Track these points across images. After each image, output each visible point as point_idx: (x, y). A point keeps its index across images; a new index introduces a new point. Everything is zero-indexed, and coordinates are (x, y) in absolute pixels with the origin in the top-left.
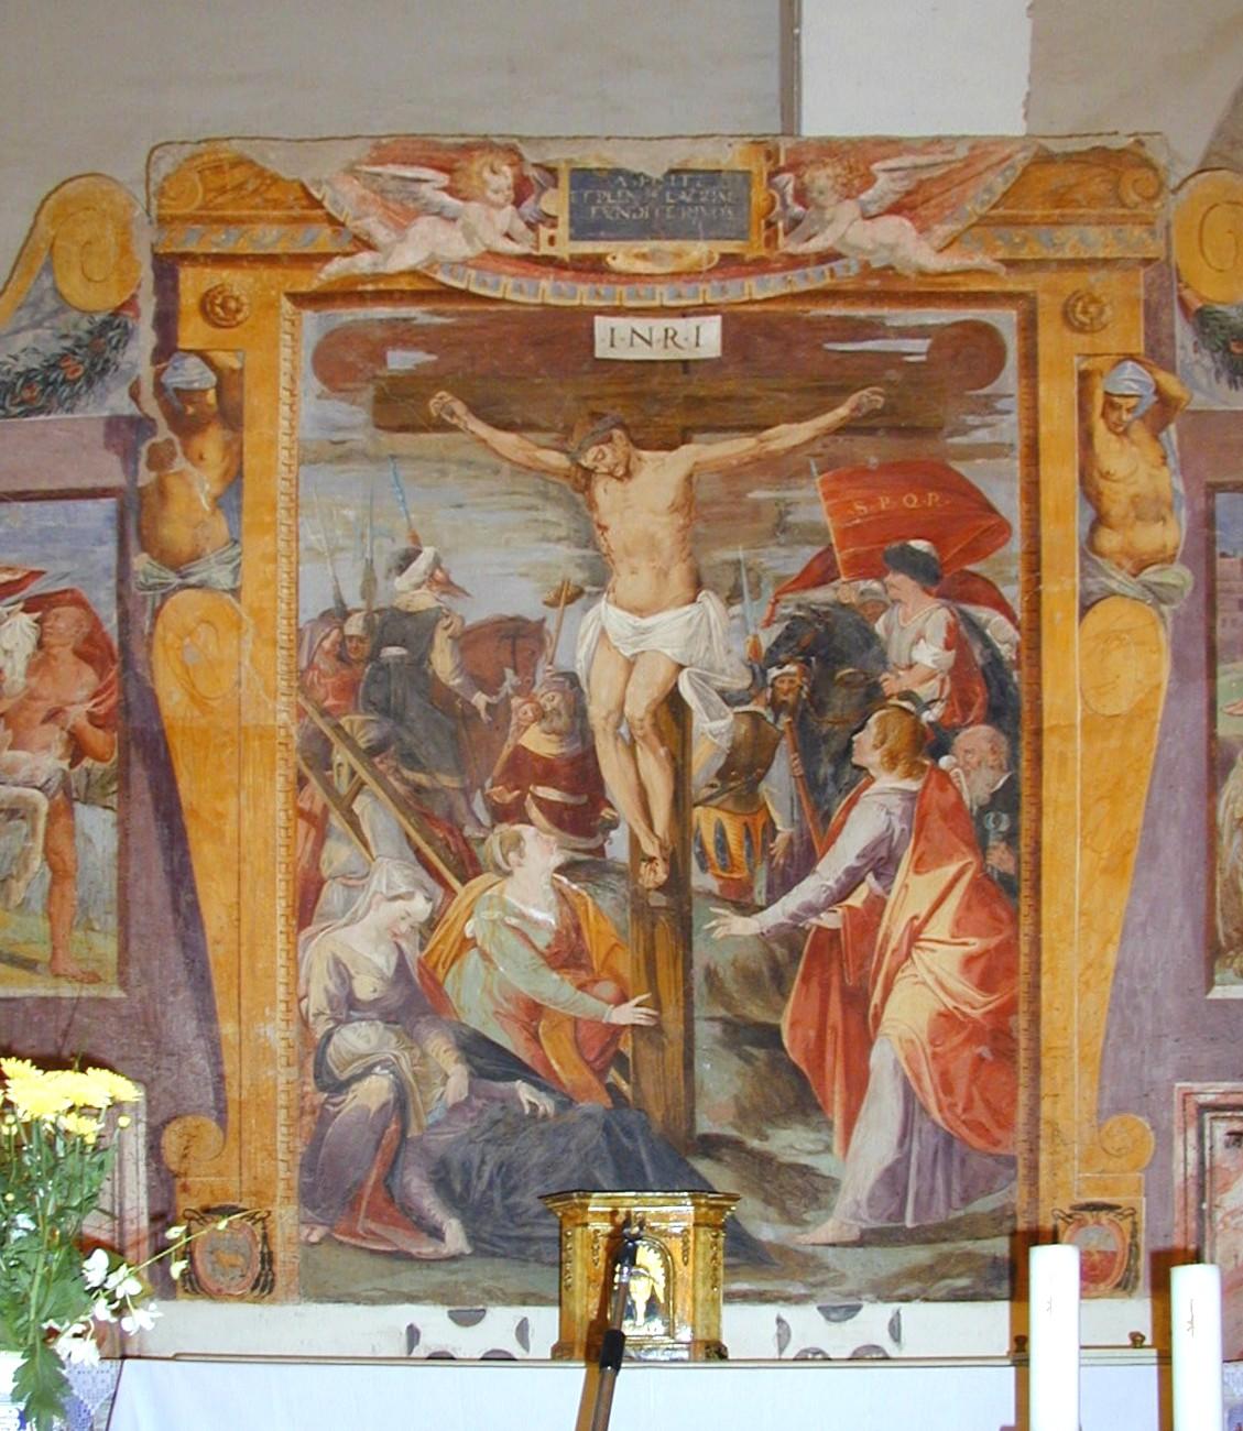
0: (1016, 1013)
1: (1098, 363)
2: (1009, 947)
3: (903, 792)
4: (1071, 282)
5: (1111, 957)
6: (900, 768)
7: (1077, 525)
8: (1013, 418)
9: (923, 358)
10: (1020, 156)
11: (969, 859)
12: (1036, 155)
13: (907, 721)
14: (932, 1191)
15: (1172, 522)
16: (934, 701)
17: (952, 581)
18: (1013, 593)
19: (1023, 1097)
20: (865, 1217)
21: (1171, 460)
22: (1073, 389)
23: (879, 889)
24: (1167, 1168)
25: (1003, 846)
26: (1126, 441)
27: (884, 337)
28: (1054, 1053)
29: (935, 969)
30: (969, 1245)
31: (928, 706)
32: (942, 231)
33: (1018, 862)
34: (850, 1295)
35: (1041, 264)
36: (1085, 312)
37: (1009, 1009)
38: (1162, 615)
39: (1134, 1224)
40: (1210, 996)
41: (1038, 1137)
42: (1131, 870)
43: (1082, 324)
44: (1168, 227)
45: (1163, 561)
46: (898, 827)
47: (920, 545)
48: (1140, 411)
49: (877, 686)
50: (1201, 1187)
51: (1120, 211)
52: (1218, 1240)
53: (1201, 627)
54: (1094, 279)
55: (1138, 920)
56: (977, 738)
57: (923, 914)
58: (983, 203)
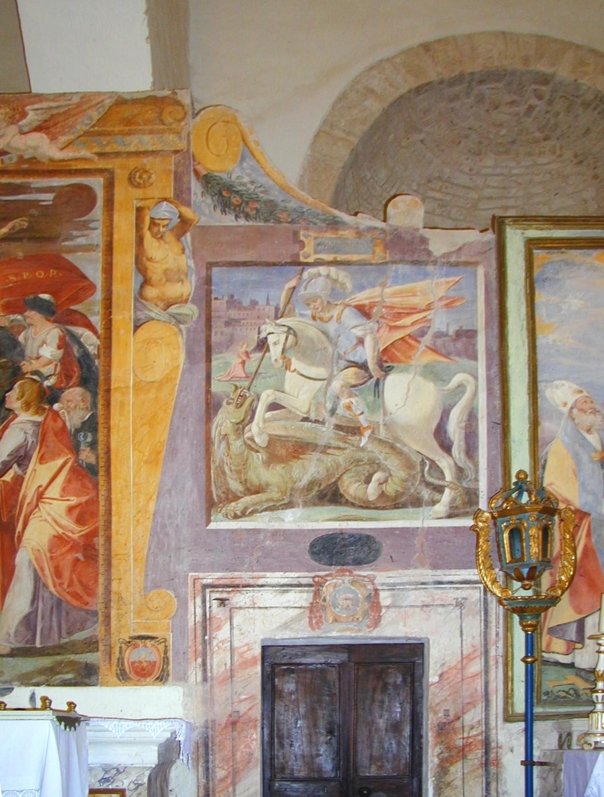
0: (97, 536)
1: (147, 203)
2: (94, 502)
3: (34, 422)
4: (133, 163)
5: (152, 507)
6: (31, 410)
7: (134, 282)
8: (99, 231)
9: (51, 203)
10: (108, 101)
11: (69, 456)
12: (116, 100)
13: (36, 386)
14: (51, 627)
15: (187, 284)
16: (51, 375)
17: (63, 314)
18: (97, 320)
19: (101, 580)
20: (13, 641)
21: (187, 251)
22: (133, 216)
23: (20, 472)
24: (184, 618)
25: (88, 449)
26: (162, 242)
27: (30, 193)
28: (119, 557)
29: (52, 513)
30: (72, 657)
31: (47, 378)
32: (63, 139)
33: (97, 458)
34: (6, 682)
35: (117, 154)
36: (140, 177)
37: (94, 533)
38: (180, 330)
39: (166, 647)
40: (208, 528)
41: (110, 601)
42: (161, 462)
43: (139, 184)
44: (189, 134)
45: (181, 302)
46: (30, 440)
47: (45, 296)
48: (170, 227)
49: (19, 368)
50: (204, 628)
51: (162, 127)
52: (215, 656)
53: (203, 336)
54: (146, 161)
55: (167, 488)
56: (74, 394)
57: (45, 484)
58: (86, 125)
